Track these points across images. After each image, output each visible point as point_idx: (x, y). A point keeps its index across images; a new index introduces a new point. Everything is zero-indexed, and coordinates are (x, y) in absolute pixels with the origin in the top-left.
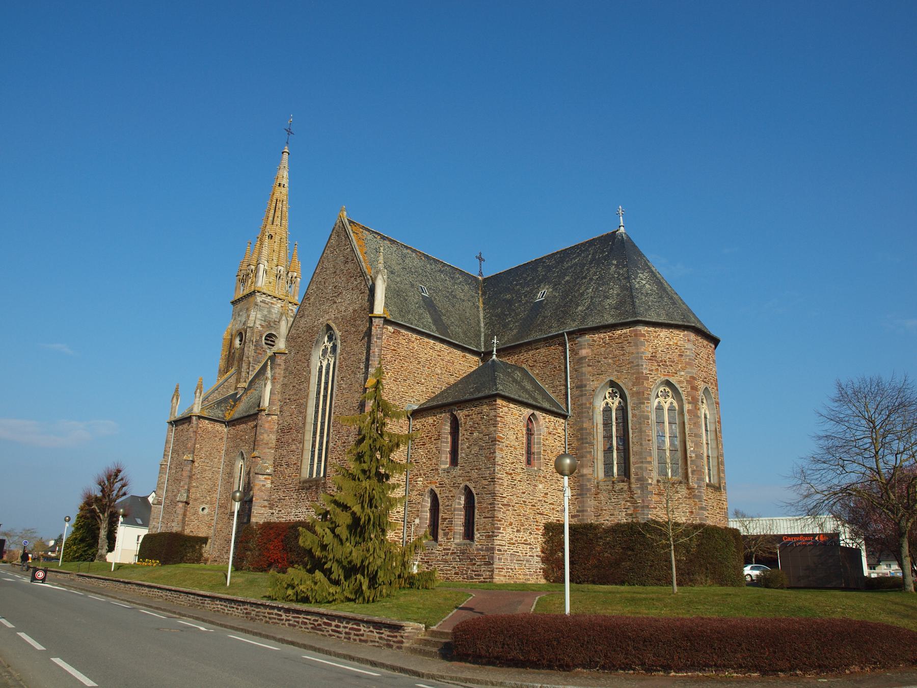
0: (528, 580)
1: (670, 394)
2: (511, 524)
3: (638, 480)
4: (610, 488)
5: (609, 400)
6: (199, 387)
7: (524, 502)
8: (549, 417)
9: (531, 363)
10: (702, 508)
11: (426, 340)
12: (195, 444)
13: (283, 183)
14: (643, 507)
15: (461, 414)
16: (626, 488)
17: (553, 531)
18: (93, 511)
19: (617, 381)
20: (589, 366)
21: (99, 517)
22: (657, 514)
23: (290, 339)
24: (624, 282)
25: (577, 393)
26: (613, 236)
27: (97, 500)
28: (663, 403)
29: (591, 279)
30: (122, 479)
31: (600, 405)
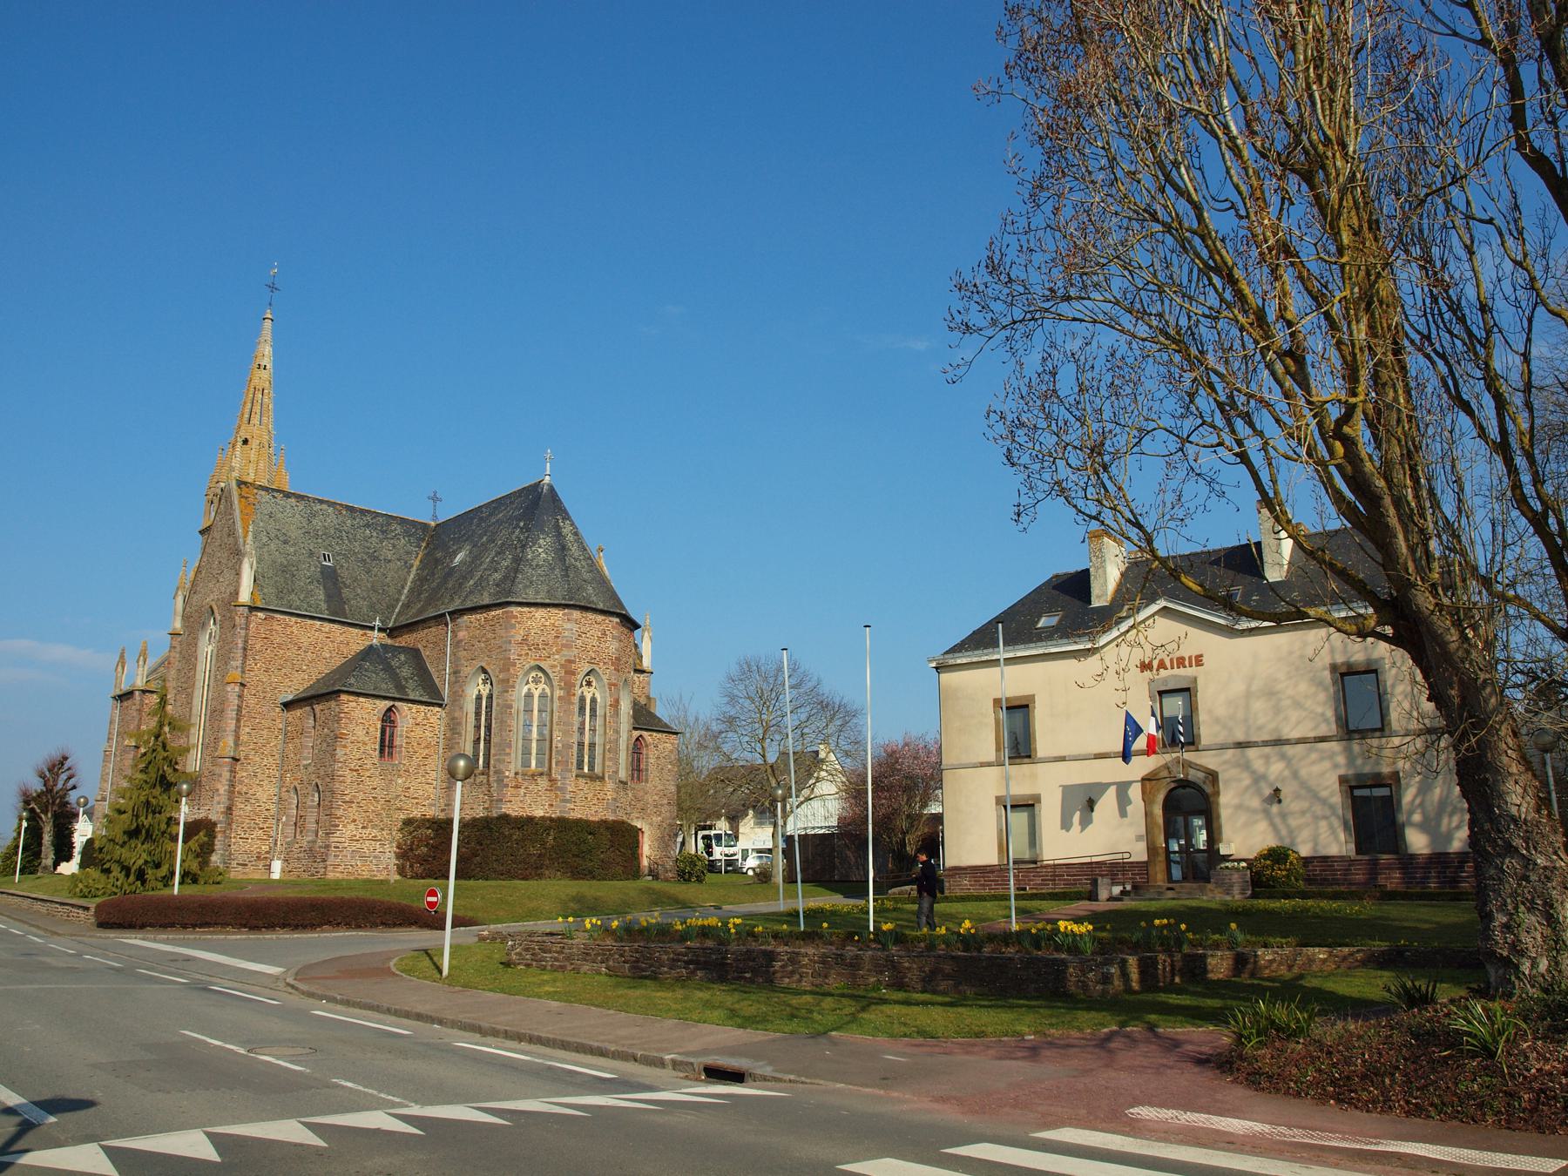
5: (481, 687)
6: (144, 654)
15: (317, 708)
22: (513, 809)
31: (471, 692)
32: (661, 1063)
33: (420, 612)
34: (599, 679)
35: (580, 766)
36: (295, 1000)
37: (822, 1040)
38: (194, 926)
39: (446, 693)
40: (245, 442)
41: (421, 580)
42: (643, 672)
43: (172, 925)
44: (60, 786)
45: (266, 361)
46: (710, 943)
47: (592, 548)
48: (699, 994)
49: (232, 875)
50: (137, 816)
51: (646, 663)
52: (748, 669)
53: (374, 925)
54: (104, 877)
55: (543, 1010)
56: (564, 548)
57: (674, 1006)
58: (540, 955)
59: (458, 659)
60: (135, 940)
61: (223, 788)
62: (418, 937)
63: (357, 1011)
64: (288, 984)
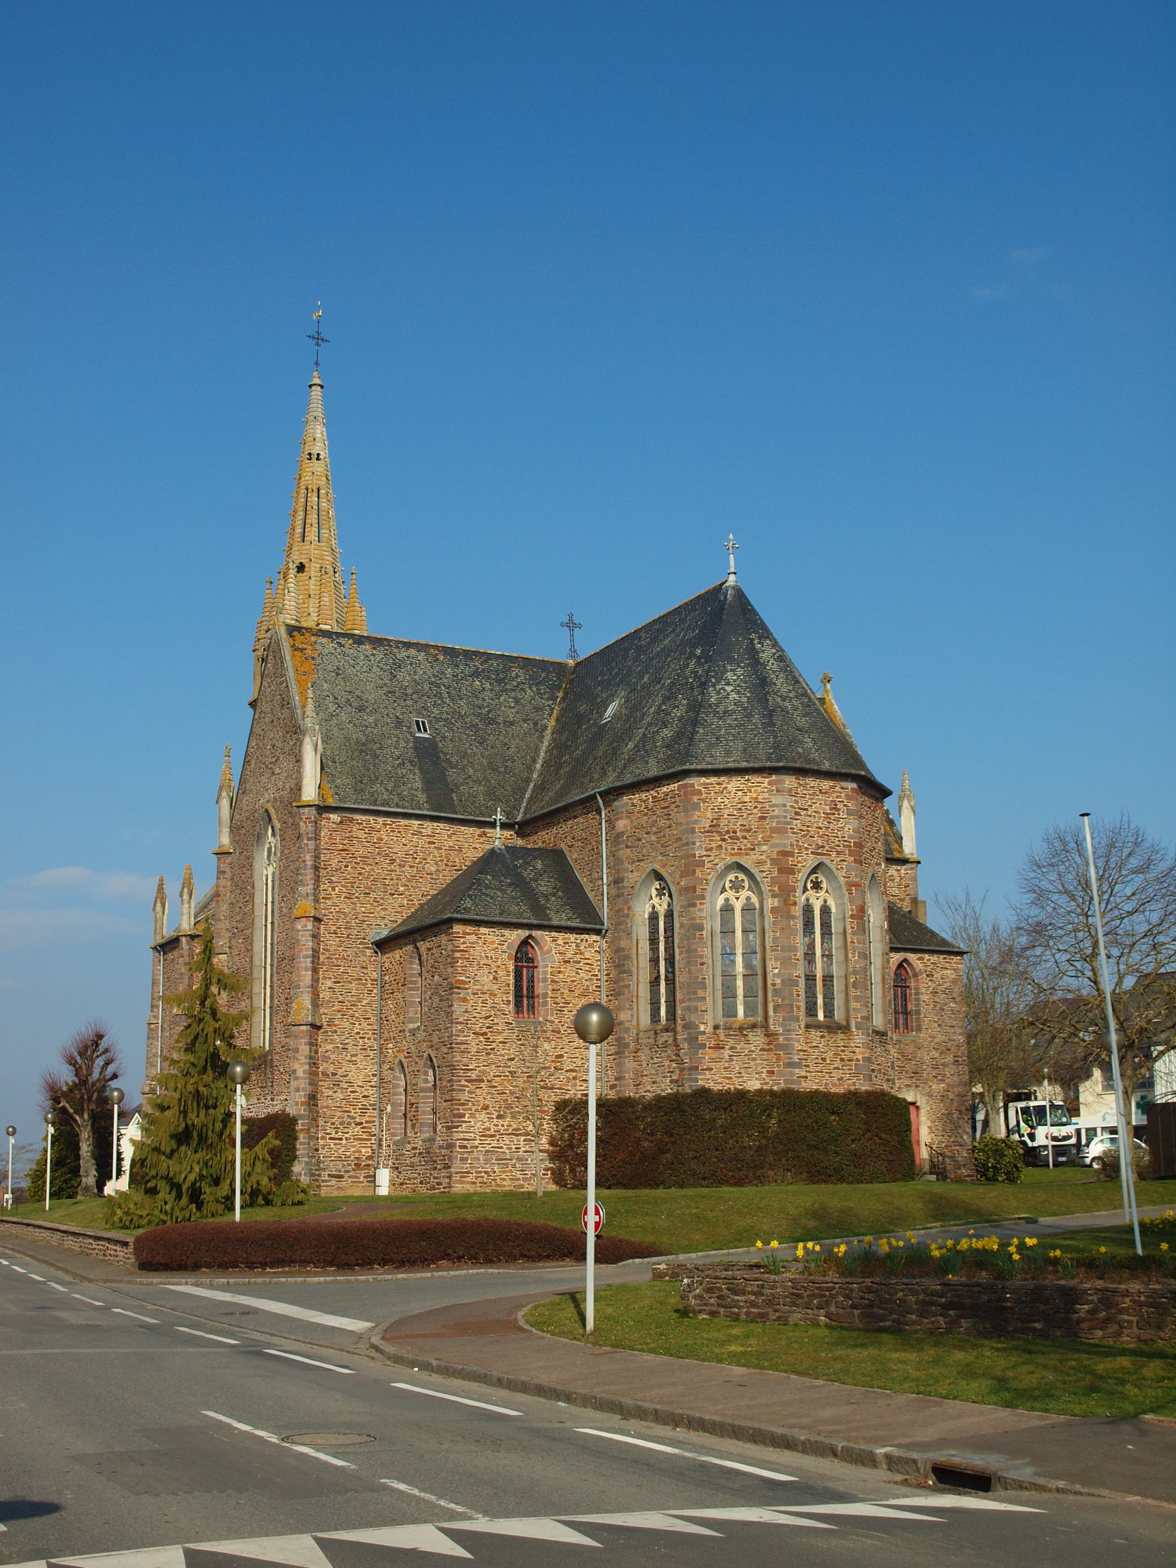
0: (522, 1186)
1: (746, 884)
2: (486, 1107)
4: (652, 1041)
5: (656, 901)
6: (188, 884)
8: (561, 937)
9: (569, 841)
11: (404, 822)
13: (314, 452)
14: (690, 1069)
15: (423, 946)
16: (671, 1040)
17: (571, 1110)
18: (64, 1110)
19: (662, 871)
20: (627, 847)
21: (76, 1121)
22: (715, 1079)
25: (614, 892)
28: (733, 901)
30: (106, 1051)
31: (642, 910)
32: (869, 1460)
33: (560, 795)
34: (831, 876)
35: (811, 1010)
36: (377, 1368)
37: (1125, 1427)
38: (264, 1265)
39: (605, 912)
40: (301, 568)
41: (559, 747)
42: (904, 861)
43: (234, 1265)
45: (318, 448)
46: (984, 1276)
47: (811, 678)
48: (959, 1355)
49: (324, 1192)
50: (185, 1113)
51: (909, 847)
53: (511, 1259)
54: (148, 1200)
55: (721, 1381)
56: (763, 682)
57: (914, 1373)
58: (733, 1300)
59: (619, 861)
60: (186, 1287)
61: (301, 1069)
62: (553, 1276)
63: (457, 1383)
64: (373, 1346)
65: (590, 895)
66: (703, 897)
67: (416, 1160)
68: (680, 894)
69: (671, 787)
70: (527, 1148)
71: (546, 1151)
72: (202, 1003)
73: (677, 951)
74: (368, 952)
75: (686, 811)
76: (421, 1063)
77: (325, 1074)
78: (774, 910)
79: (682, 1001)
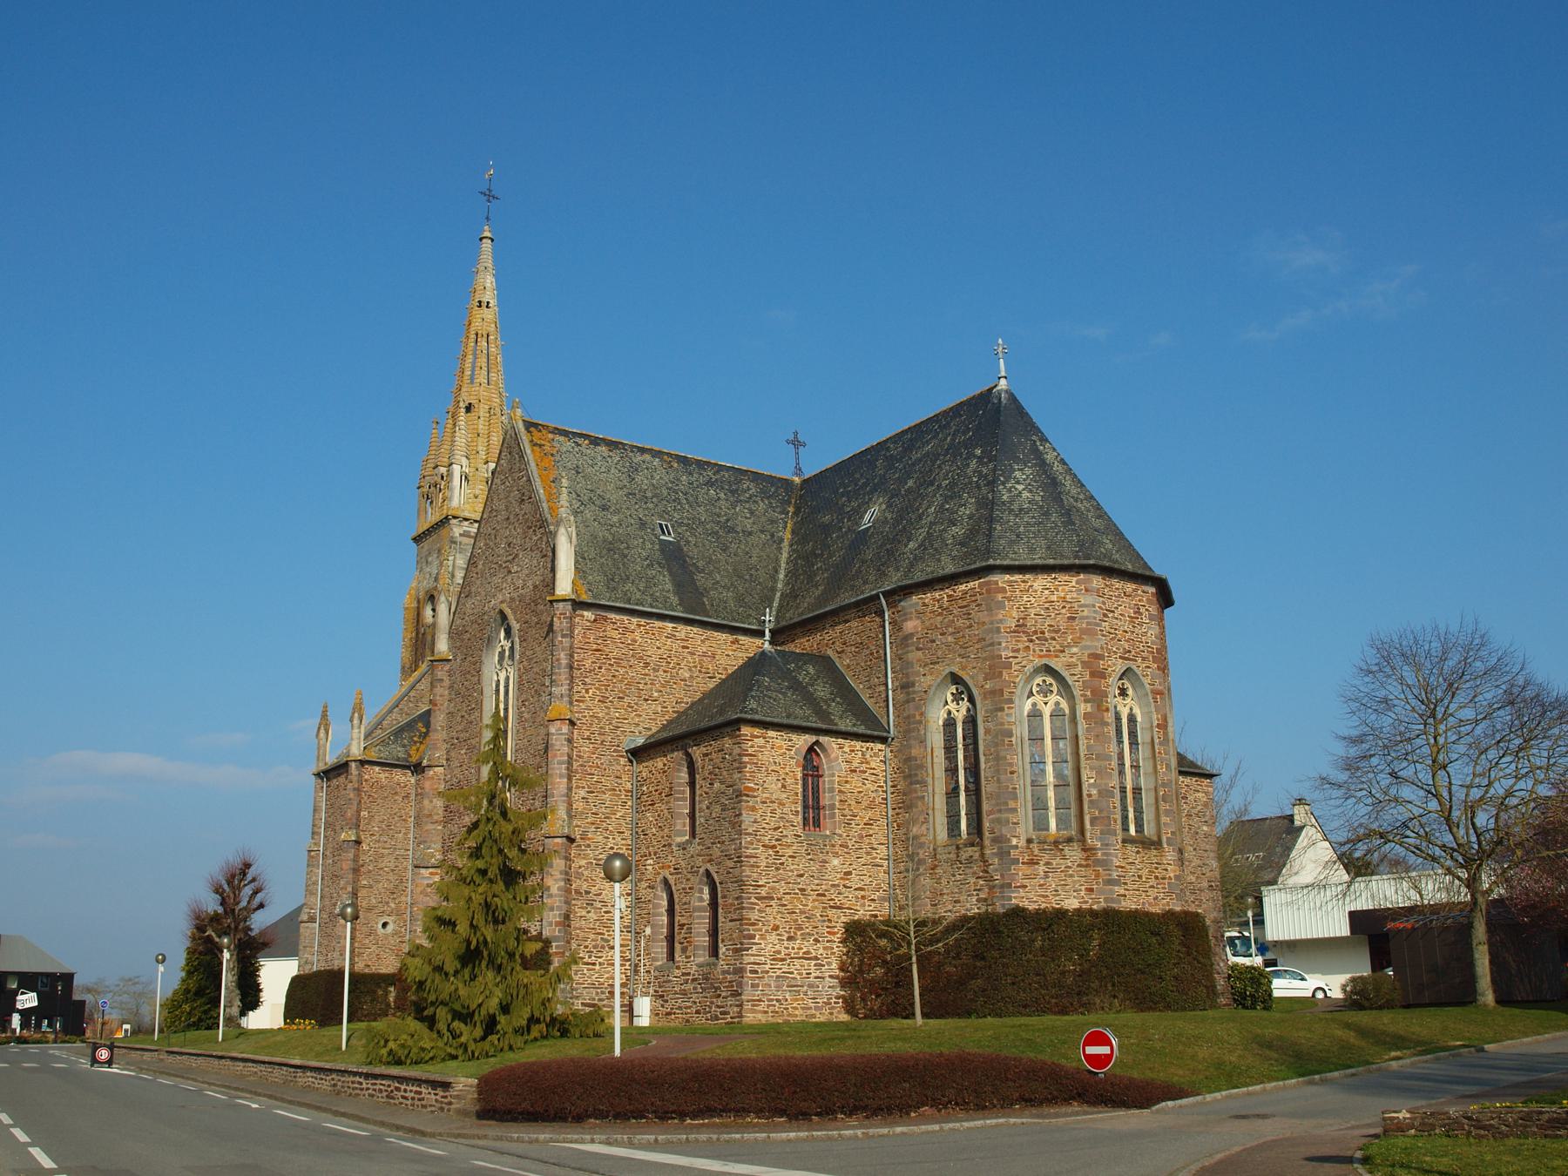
0: (813, 1016)
1: (1055, 689)
2: (776, 928)
3: (995, 840)
4: (953, 856)
5: (952, 706)
6: (358, 709)
7: (802, 890)
8: (848, 744)
10: (1110, 882)
11: (658, 624)
12: (359, 811)
13: (485, 300)
14: (1002, 886)
15: (697, 752)
19: (960, 673)
23: (454, 634)
24: (984, 490)
25: (902, 697)
26: (986, 398)
27: (215, 919)
28: (1041, 706)
29: (939, 486)
30: (254, 880)
31: (937, 716)
38: (682, 1115)
40: (469, 409)
43: (639, 1115)
44: (244, 904)
52: (1389, 657)
56: (1054, 483)
65: (869, 703)
66: (1011, 701)
67: (690, 986)
68: (985, 698)
69: (971, 585)
70: (818, 974)
71: (837, 977)
72: (490, 803)
73: (982, 759)
74: (623, 761)
75: (990, 609)
76: (695, 880)
77: (578, 892)
78: (1086, 716)
79: (990, 813)
